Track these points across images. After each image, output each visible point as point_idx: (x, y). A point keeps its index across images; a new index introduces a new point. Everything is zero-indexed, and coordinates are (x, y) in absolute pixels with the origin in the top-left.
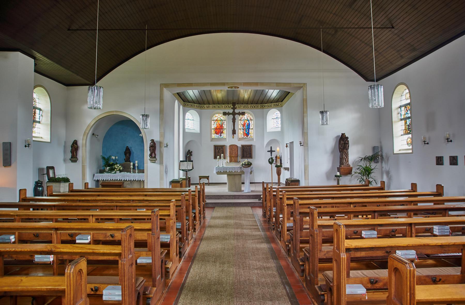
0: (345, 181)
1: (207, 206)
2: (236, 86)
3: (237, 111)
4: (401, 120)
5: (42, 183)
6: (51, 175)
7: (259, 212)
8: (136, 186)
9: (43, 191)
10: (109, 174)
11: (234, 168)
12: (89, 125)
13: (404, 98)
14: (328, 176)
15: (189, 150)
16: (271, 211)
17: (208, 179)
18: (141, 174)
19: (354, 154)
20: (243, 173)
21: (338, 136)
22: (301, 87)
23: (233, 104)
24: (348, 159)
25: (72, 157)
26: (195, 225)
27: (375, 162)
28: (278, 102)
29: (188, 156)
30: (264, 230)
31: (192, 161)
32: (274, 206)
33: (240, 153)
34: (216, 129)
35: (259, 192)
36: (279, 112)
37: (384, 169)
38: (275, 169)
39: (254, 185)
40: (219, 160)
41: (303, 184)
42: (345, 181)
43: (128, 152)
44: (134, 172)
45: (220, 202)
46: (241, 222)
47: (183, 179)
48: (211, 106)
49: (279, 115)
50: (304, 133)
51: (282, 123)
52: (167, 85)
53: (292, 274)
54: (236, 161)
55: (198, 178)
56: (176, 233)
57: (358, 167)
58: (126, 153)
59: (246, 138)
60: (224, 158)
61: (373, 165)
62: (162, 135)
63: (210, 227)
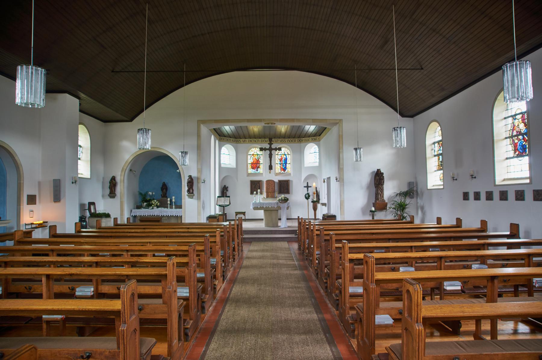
0: (380, 216)
1: (244, 241)
2: (273, 122)
3: (273, 146)
4: (435, 156)
5: (85, 218)
6: (93, 211)
7: (295, 246)
8: (173, 221)
9: (86, 225)
10: (147, 210)
11: (271, 203)
12: (127, 161)
13: (437, 134)
14: (364, 211)
15: (225, 186)
16: (304, 242)
17: (244, 215)
18: (178, 210)
19: (390, 190)
20: (279, 208)
21: (373, 172)
22: (337, 122)
23: (270, 139)
24: (383, 194)
25: (110, 193)
26: (234, 256)
27: (410, 198)
28: (316, 136)
29: (224, 192)
30: (298, 260)
31: (229, 197)
32: (308, 238)
33: (277, 188)
34: (252, 164)
35: (295, 227)
36: (316, 147)
37: (419, 205)
38: (311, 205)
39: (291, 220)
40: (256, 196)
41: (339, 219)
42: (380, 216)
43: (165, 188)
44: (171, 208)
45: (256, 237)
46: (277, 254)
47: (220, 215)
48: (247, 140)
49: (317, 149)
50: (340, 169)
51: (320, 159)
52: (204, 122)
53: (318, 291)
54: (273, 197)
55: (235, 214)
56: (220, 258)
57: (393, 202)
58: (162, 189)
59: (283, 173)
60: (261, 193)
61: (408, 201)
62: (200, 171)
63: (248, 258)
